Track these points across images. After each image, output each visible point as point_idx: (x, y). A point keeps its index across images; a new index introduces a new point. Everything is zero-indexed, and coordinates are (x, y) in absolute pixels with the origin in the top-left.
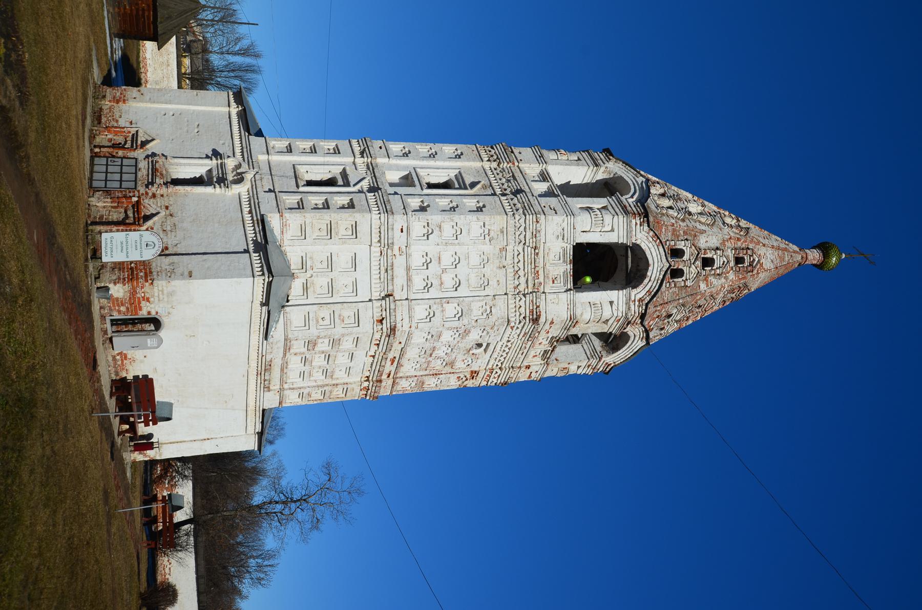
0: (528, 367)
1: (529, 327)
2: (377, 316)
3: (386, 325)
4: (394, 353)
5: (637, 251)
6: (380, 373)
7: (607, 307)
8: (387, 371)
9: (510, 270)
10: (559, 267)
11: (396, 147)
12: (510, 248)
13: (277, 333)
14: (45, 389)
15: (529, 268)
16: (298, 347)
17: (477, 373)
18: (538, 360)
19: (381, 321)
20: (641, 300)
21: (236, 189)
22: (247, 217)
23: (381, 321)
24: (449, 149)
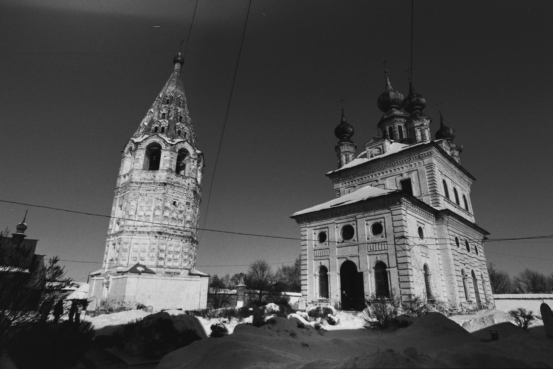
0: (189, 184)
1: (168, 186)
2: (154, 237)
3: (157, 235)
4: (172, 232)
5: (149, 148)
6: (181, 236)
7: (166, 158)
8: (180, 234)
9: (148, 192)
10: (149, 175)
11: (110, 226)
12: (140, 192)
13: (154, 270)
14: (185, 265)
15: (148, 186)
16: (161, 263)
17: (187, 203)
18: (187, 181)
19: (156, 237)
20: (166, 146)
21: (111, 280)
22: (117, 277)
23: (156, 237)
24: (113, 208)
